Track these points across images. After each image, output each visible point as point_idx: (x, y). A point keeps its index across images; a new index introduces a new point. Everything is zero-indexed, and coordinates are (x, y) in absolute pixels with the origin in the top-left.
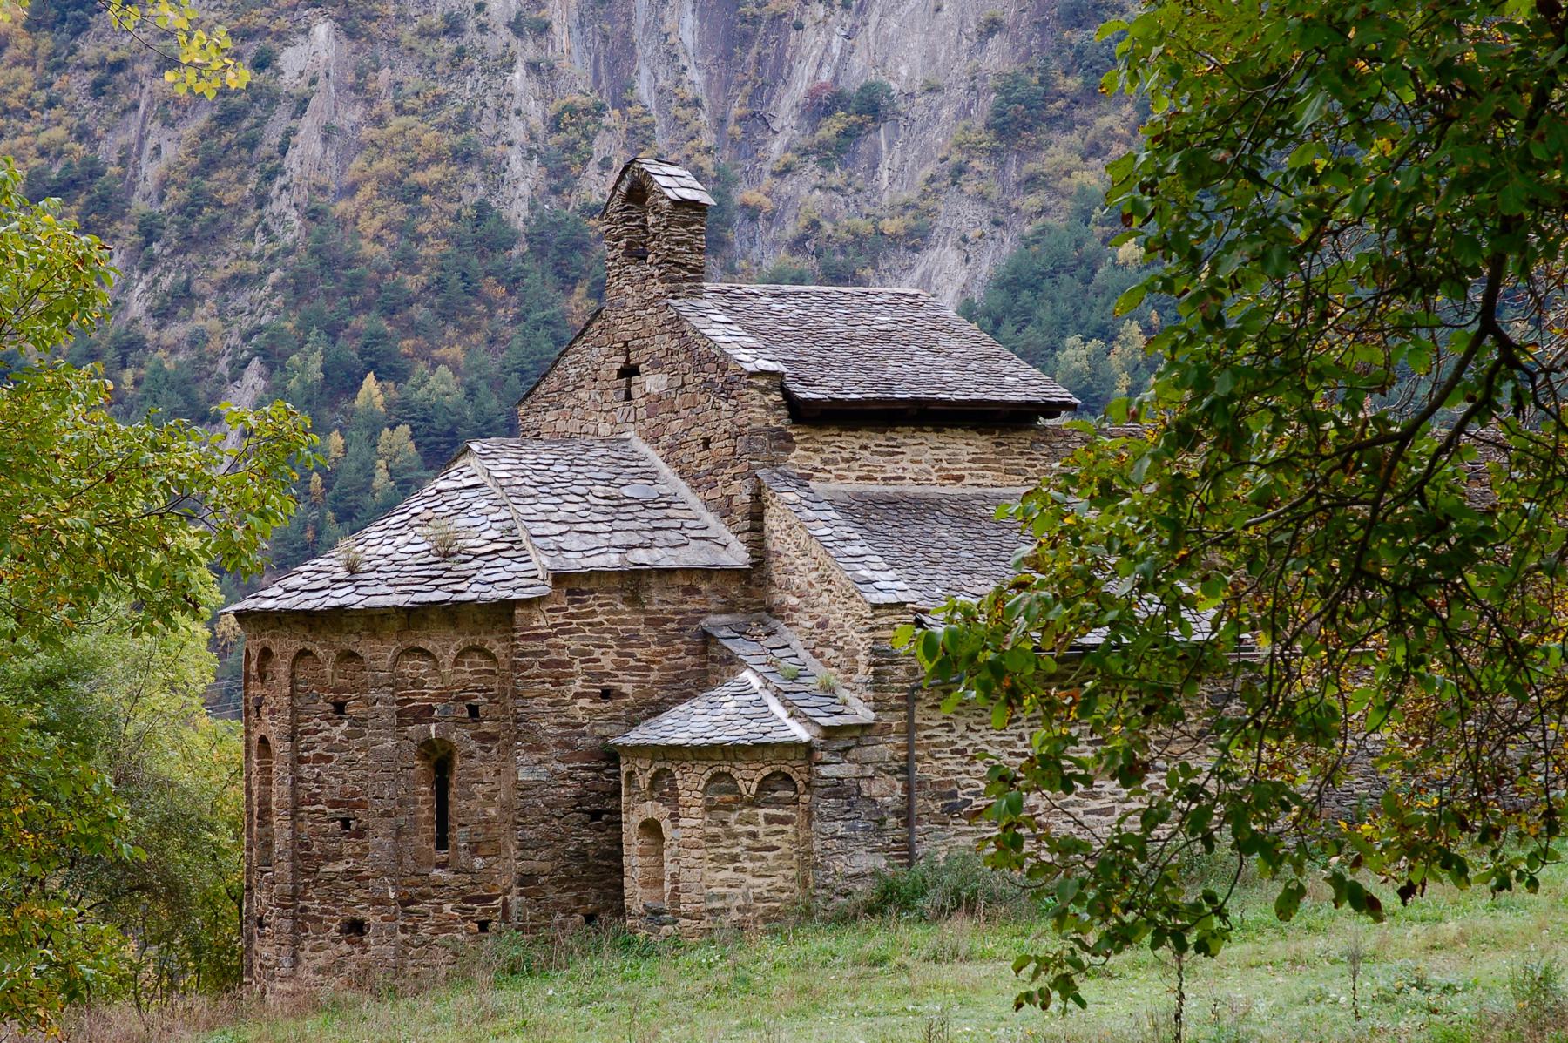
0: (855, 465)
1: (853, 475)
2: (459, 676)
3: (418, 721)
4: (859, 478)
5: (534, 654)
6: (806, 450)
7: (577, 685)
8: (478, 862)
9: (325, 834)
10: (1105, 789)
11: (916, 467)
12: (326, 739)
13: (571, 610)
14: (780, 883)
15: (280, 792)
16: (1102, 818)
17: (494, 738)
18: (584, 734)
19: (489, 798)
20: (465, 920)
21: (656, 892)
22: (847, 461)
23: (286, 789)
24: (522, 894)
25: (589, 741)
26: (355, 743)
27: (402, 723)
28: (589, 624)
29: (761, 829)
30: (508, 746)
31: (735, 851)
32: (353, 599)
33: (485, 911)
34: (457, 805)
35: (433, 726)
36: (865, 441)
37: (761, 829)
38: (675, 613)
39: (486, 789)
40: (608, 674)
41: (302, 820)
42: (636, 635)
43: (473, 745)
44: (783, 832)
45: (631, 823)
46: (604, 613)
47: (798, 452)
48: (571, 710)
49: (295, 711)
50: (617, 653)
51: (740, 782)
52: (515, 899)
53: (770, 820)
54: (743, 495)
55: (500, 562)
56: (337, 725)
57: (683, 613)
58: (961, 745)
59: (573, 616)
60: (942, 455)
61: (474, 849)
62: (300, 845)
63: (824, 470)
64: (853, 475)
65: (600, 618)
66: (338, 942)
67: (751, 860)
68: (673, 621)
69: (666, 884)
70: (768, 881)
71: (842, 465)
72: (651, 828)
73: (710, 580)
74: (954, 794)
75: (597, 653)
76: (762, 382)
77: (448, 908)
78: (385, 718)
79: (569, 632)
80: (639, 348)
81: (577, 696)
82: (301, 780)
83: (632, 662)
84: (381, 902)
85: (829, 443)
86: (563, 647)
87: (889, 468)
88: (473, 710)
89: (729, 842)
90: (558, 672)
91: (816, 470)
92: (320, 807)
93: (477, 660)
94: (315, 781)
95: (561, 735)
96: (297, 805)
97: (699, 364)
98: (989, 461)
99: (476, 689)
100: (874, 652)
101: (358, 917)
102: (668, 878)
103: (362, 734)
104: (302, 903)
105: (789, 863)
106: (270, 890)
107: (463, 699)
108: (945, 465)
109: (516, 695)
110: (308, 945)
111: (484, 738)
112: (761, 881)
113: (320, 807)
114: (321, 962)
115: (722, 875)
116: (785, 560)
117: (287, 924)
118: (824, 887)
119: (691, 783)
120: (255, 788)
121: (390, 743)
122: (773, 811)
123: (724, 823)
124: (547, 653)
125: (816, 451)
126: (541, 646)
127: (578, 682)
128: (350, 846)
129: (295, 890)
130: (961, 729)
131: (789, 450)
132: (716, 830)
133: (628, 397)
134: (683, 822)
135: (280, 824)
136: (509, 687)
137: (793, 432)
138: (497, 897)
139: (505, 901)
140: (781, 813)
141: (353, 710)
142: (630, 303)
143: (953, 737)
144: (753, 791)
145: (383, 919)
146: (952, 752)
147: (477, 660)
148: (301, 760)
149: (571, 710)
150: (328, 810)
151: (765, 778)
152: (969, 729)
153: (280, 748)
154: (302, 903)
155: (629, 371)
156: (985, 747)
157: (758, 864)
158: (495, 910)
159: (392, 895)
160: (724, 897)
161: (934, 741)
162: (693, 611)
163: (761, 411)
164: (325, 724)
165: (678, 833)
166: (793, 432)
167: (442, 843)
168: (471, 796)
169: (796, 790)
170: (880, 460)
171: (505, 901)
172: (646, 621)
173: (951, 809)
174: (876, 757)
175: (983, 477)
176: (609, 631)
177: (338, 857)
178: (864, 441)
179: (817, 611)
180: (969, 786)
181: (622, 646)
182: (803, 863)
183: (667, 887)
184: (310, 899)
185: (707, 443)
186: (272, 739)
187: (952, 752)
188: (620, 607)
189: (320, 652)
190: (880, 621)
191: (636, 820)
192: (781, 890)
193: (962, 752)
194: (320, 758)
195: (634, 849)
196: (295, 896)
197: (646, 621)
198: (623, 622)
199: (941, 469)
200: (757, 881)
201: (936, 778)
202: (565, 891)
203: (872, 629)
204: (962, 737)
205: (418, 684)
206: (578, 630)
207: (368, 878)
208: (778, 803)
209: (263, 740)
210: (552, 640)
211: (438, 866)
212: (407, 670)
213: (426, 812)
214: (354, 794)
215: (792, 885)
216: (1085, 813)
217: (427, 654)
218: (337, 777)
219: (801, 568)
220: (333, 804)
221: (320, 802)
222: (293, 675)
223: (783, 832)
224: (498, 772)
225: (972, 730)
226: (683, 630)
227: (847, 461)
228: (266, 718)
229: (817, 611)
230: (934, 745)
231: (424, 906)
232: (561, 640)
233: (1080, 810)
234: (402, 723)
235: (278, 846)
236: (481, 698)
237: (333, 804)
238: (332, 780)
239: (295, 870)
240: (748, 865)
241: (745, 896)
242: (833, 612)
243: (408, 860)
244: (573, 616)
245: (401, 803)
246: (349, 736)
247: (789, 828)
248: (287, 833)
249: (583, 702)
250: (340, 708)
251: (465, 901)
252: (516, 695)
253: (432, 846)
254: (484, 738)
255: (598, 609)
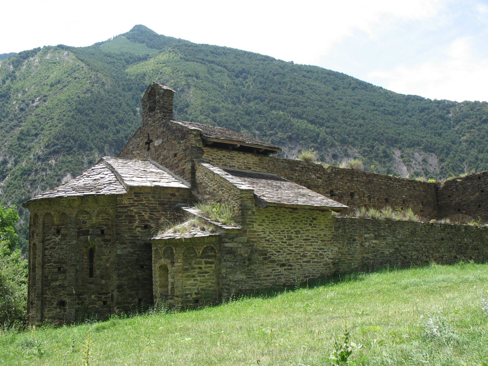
0: (222, 161)
1: (221, 164)
2: (98, 220)
3: (84, 235)
4: (222, 165)
5: (123, 212)
6: (208, 155)
7: (136, 224)
8: (103, 282)
9: (53, 273)
10: (308, 255)
11: (238, 164)
12: (53, 242)
13: (135, 199)
14: (210, 284)
15: (39, 259)
16: (307, 264)
17: (109, 241)
18: (139, 239)
19: (107, 260)
20: (99, 301)
21: (165, 289)
22: (219, 159)
23: (40, 258)
24: (118, 291)
25: (141, 242)
26: (63, 243)
27: (79, 236)
28: (141, 204)
29: (203, 266)
30: (114, 243)
31: (194, 273)
32: (64, 195)
33: (105, 298)
34: (96, 262)
35: (89, 237)
36: (224, 154)
37: (203, 266)
38: (168, 202)
39: (106, 257)
40: (147, 220)
41: (45, 268)
42: (156, 209)
43: (102, 243)
44: (210, 267)
45: (156, 267)
46: (146, 200)
47: (205, 155)
48: (135, 232)
49: (44, 233)
50: (150, 214)
51: (196, 250)
52: (115, 293)
53: (206, 263)
54: (189, 166)
55: (111, 185)
56: (57, 237)
57: (170, 202)
58: (268, 238)
59: (136, 201)
60: (245, 161)
61: (102, 278)
62: (44, 277)
63: (212, 161)
64: (221, 164)
65: (144, 202)
66: (56, 308)
67: (200, 276)
68: (167, 204)
69: (169, 286)
70: (206, 284)
71: (218, 161)
72: (164, 269)
73: (179, 192)
74: (266, 254)
75: (143, 213)
76: (195, 133)
77: (93, 297)
78: (73, 234)
79: (135, 206)
80: (152, 134)
81: (137, 227)
82: (46, 255)
83: (154, 217)
84: (71, 294)
85: (214, 154)
86: (133, 211)
87: (231, 163)
88: (103, 232)
89: (192, 270)
90: (131, 219)
91: (210, 161)
92: (51, 264)
93: (104, 215)
94: (50, 255)
95: (131, 239)
96: (44, 263)
97: (173, 132)
98: (257, 164)
99: (103, 225)
100: (241, 205)
101: (63, 300)
102: (170, 284)
103: (65, 239)
104: (45, 296)
105: (213, 277)
106: (35, 292)
107: (99, 228)
108: (246, 164)
109: (117, 225)
110: (46, 310)
111: (106, 241)
112: (203, 284)
113: (51, 264)
114: (50, 315)
115: (189, 282)
116: (204, 184)
117: (40, 302)
118: (227, 285)
119: (178, 253)
120: (31, 260)
121: (75, 242)
122: (208, 260)
123: (190, 264)
124: (127, 212)
125: (211, 155)
126: (125, 210)
127: (137, 222)
128: (61, 277)
129: (42, 291)
130: (268, 233)
131: (203, 154)
132: (187, 267)
133: (149, 149)
134: (176, 264)
135: (39, 271)
136: (114, 224)
137: (204, 149)
138: (109, 293)
139: (112, 294)
140: (210, 260)
141: (63, 231)
142: (150, 122)
143: (265, 235)
144: (201, 253)
145: (71, 300)
146: (265, 240)
147: (104, 215)
148: (46, 249)
149: (135, 232)
150: (54, 265)
151: (205, 248)
152: (270, 233)
153: (39, 246)
154: (45, 296)
155: (149, 142)
156: (275, 239)
157: (202, 278)
158: (109, 298)
159: (74, 292)
160: (190, 289)
161: (260, 236)
162: (174, 201)
163: (193, 141)
164: (54, 237)
165: (174, 268)
166: (204, 149)
167: (91, 274)
168: (101, 260)
169: (215, 253)
170: (228, 160)
171: (112, 294)
172: (159, 204)
173: (265, 259)
174: (242, 241)
175: (256, 169)
176: (146, 206)
177: (57, 280)
178: (224, 154)
179: (216, 198)
180: (270, 252)
181: (152, 211)
182: (218, 278)
183: (170, 287)
184: (47, 294)
185: (175, 155)
186: (37, 243)
187: (265, 240)
188: (151, 199)
189: (53, 213)
190: (243, 195)
191: (158, 265)
192: (210, 287)
193: (268, 241)
194: (52, 248)
195: (157, 275)
196: (42, 294)
197: (159, 204)
198: (152, 204)
199: (245, 165)
200: (201, 284)
201: (261, 249)
202: (132, 291)
203: (241, 198)
204: (268, 236)
205: (84, 222)
206: (137, 206)
207: (66, 287)
208: (209, 257)
209: (34, 244)
210: (129, 208)
211: (90, 283)
212: (81, 218)
213: (86, 265)
214: (63, 259)
215: (214, 285)
216: (303, 262)
217: (87, 213)
218: (57, 254)
219: (210, 185)
220: (55, 262)
221: (51, 262)
222: (44, 221)
223: (210, 267)
224: (110, 252)
225: (271, 234)
226: (171, 207)
227: (219, 159)
228: (35, 237)
229: (216, 198)
230: (260, 238)
231: (85, 296)
232: (132, 208)
233: (301, 261)
234: (79, 236)
235: (37, 278)
236: (105, 228)
237: (55, 262)
238: (55, 255)
239: (42, 284)
240: (199, 278)
241: (198, 289)
242: (224, 196)
243: (80, 281)
244: (136, 201)
245: (78, 262)
246: (61, 240)
247: (213, 265)
248: (40, 273)
249: (139, 229)
250: (58, 232)
251: (99, 294)
252: (117, 225)
253: (88, 277)
254: (106, 241)
255: (143, 199)
